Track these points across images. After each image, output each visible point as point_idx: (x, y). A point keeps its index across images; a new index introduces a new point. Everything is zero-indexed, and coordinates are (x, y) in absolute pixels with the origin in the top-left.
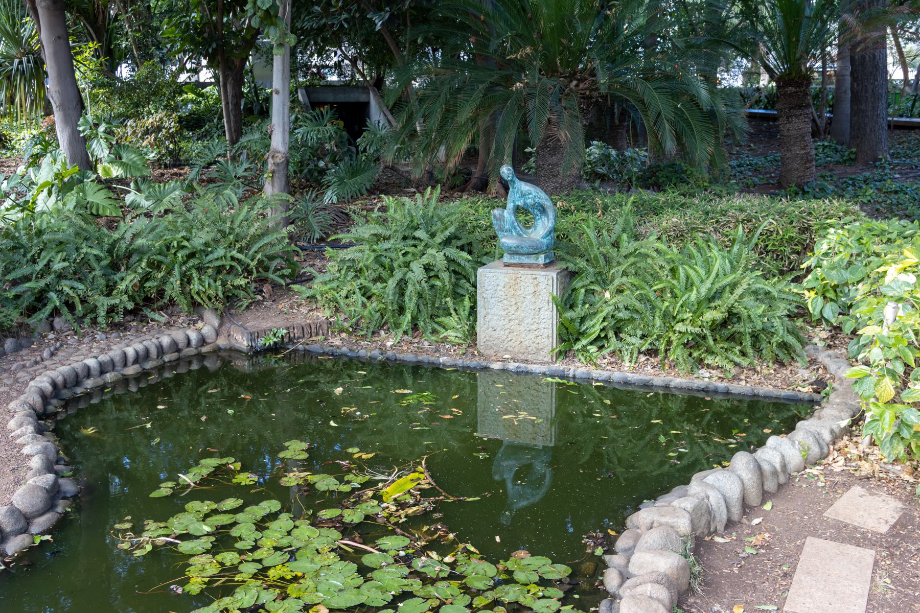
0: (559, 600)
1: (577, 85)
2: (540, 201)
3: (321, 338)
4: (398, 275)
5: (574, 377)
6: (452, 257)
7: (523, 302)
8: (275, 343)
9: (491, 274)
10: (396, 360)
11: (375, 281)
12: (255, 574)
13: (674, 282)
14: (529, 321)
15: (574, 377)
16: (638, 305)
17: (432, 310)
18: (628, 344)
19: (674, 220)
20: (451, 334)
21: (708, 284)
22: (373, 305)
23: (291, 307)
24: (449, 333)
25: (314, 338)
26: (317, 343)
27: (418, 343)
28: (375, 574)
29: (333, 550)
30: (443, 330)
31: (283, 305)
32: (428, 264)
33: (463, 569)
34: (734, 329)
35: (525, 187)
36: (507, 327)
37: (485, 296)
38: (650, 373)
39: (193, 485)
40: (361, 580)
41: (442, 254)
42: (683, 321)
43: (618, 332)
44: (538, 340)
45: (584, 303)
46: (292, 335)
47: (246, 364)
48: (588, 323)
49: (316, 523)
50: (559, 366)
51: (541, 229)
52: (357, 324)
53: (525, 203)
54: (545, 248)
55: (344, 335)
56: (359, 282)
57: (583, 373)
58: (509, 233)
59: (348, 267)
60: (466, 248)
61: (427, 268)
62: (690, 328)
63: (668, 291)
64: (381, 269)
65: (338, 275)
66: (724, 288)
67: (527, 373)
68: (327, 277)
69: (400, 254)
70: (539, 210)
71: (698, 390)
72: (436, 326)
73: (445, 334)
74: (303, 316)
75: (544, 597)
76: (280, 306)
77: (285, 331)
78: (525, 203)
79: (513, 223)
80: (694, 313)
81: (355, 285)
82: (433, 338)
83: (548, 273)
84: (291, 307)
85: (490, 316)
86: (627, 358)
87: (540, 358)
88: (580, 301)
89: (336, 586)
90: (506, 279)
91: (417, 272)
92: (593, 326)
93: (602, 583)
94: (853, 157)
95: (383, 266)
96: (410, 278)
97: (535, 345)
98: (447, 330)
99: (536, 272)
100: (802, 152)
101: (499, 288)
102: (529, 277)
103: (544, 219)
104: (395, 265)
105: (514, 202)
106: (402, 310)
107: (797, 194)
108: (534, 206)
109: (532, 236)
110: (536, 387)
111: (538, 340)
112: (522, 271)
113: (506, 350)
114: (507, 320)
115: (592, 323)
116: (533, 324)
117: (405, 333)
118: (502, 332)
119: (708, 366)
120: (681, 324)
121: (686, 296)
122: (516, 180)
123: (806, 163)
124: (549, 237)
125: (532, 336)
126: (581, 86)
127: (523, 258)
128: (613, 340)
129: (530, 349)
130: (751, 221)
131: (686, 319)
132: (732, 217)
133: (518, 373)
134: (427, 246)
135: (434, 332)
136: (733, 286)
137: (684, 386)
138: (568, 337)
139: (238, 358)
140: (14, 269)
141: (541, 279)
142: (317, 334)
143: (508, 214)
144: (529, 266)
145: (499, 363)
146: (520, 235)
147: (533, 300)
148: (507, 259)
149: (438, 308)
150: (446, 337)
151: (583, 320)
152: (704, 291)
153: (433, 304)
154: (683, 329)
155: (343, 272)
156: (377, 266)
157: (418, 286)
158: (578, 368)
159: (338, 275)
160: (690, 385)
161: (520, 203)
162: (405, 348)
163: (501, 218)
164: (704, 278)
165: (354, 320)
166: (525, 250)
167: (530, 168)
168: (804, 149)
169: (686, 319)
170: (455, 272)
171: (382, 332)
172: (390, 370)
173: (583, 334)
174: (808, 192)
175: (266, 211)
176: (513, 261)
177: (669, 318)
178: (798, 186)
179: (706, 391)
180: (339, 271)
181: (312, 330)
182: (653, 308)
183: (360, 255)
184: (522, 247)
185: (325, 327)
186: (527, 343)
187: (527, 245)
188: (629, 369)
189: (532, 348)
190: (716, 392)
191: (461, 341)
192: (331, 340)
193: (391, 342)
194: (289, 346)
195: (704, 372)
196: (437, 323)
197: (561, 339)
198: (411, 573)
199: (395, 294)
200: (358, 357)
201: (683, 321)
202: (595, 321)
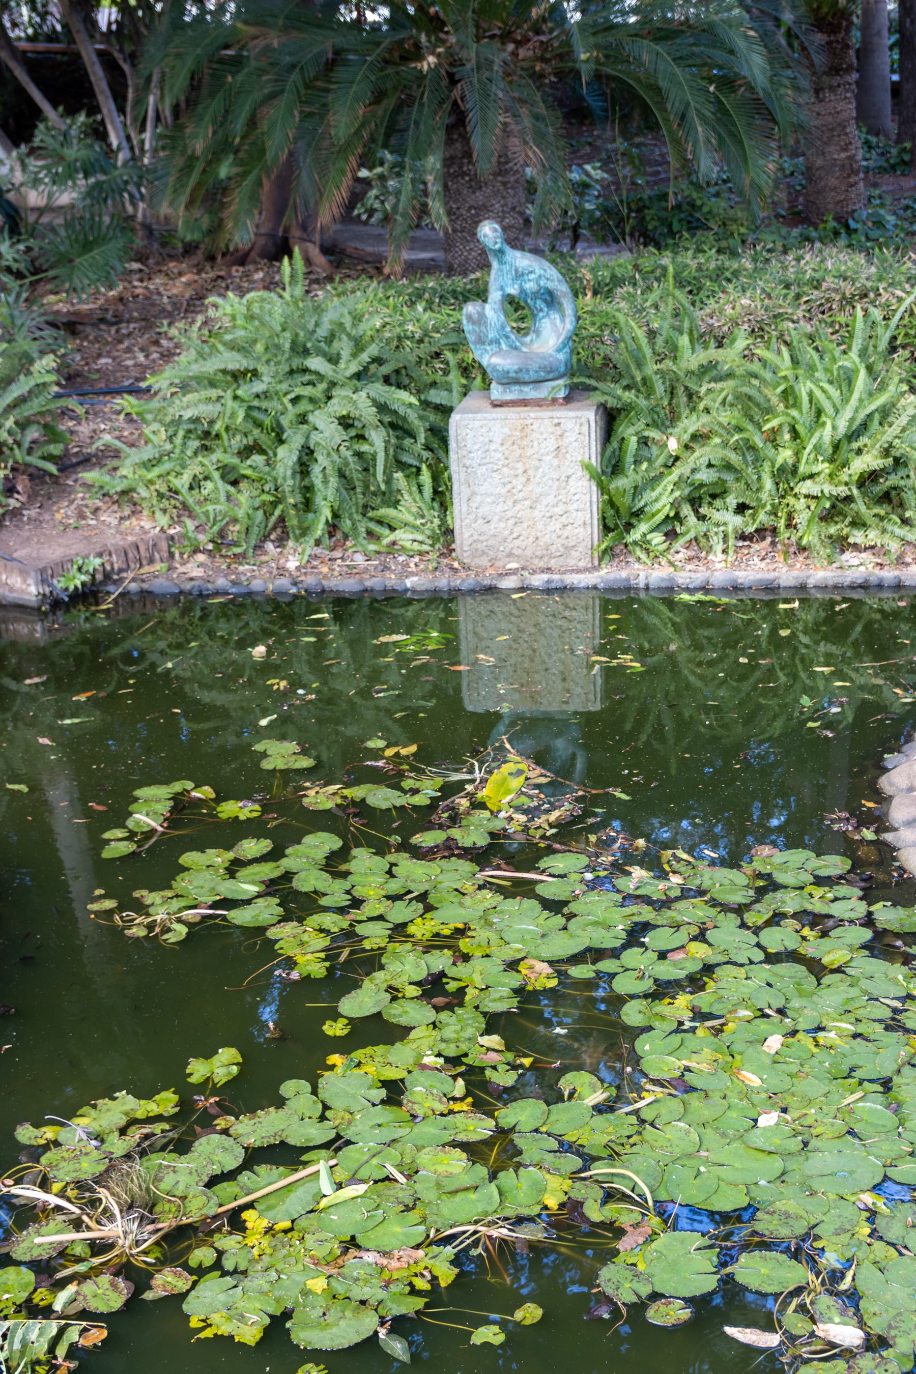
0: (861, 899)
1: (515, 54)
2: (550, 285)
3: (159, 566)
4: (295, 440)
5: (647, 588)
6: (382, 400)
7: (537, 469)
8: (84, 584)
9: (478, 424)
10: (323, 591)
11: (246, 452)
12: (390, 937)
13: (794, 413)
14: (551, 499)
15: (647, 588)
16: (734, 458)
17: (366, 497)
18: (717, 525)
19: (745, 301)
20: (403, 537)
21: (847, 413)
22: (245, 497)
23: (82, 516)
24: (399, 535)
25: (146, 569)
26: (158, 576)
27: (342, 558)
28: (573, 907)
29: (480, 888)
30: (387, 531)
31: (63, 512)
32: (348, 416)
33: (698, 882)
34: (888, 483)
35: (521, 260)
36: (509, 514)
37: (468, 463)
38: (757, 568)
39: (160, 829)
40: (560, 920)
41: (363, 394)
42: (812, 476)
43: (695, 502)
44: (566, 533)
45: (637, 462)
46: (108, 568)
47: (38, 628)
48: (649, 496)
49: (418, 853)
50: (609, 574)
51: (551, 336)
52: (222, 534)
53: (522, 290)
54: (562, 369)
55: (201, 557)
56: (214, 457)
57: (663, 580)
58: (494, 348)
59: (189, 431)
60: (393, 379)
61: (345, 422)
62: (828, 489)
63: (786, 429)
64: (256, 432)
65: (168, 447)
66: (870, 416)
67: (563, 590)
68: (148, 453)
69: (286, 400)
70: (545, 301)
71: (852, 587)
72: (373, 526)
73: (392, 537)
74: (115, 530)
75: (836, 899)
76: (58, 516)
77: (98, 561)
78: (522, 290)
79: (503, 328)
80: (831, 461)
81: (210, 461)
82: (372, 547)
83: (579, 413)
84: (82, 516)
86: (719, 547)
87: (572, 562)
88: (629, 459)
89: (529, 932)
90: (506, 430)
91: (326, 430)
92: (656, 500)
93: (901, 869)
94: (907, 157)
95: (259, 425)
96: (317, 444)
97: (561, 541)
98: (392, 529)
100: (843, 155)
101: (493, 446)
102: (547, 422)
103: (556, 316)
104: (285, 421)
105: (502, 288)
106: (307, 505)
107: (836, 234)
108: (536, 295)
109: (536, 348)
111: (566, 533)
112: (531, 414)
113: (510, 555)
115: (654, 494)
116: (556, 505)
117: (318, 543)
118: (502, 525)
119: (855, 547)
120: (809, 482)
121: (817, 435)
122: (507, 249)
123: (849, 176)
124: (567, 350)
125: (555, 525)
126: (522, 53)
127: (526, 389)
128: (692, 519)
129: (553, 549)
130: (866, 296)
131: (818, 474)
132: (836, 291)
133: (548, 591)
134: (333, 384)
136: (886, 413)
137: (830, 583)
138: (617, 521)
139: (15, 620)
141: (568, 425)
142: (151, 561)
143: (492, 311)
144: (538, 403)
145: (513, 578)
146: (516, 348)
147: (556, 462)
148: (497, 392)
149: (374, 494)
150: (394, 543)
151: (637, 491)
152: (843, 425)
153: (367, 487)
154: (815, 491)
155: (178, 440)
156: (250, 426)
157: (335, 457)
158: (645, 573)
159: (168, 447)
160: (840, 580)
161: (513, 290)
162: (325, 570)
163: (480, 320)
164: (838, 401)
165: (216, 528)
166: (533, 376)
167: (371, 212)
168: (845, 150)
169: (818, 474)
170: (393, 426)
171: (269, 546)
172: (284, 612)
173: (638, 514)
174: (856, 231)
175: (336, 344)
176: (509, 397)
177: (787, 475)
178: (837, 219)
179: (864, 586)
180: (171, 438)
181: (137, 555)
182: (758, 460)
183: (218, 407)
184: (528, 371)
185: (164, 545)
187: (535, 366)
188: (716, 565)
190: (880, 586)
191: (425, 548)
192: (182, 569)
193: (291, 565)
194: (111, 588)
195: (849, 557)
196: (371, 519)
197: (607, 529)
198: (624, 898)
199: (294, 474)
200: (250, 594)
201: (812, 476)
202: (659, 490)
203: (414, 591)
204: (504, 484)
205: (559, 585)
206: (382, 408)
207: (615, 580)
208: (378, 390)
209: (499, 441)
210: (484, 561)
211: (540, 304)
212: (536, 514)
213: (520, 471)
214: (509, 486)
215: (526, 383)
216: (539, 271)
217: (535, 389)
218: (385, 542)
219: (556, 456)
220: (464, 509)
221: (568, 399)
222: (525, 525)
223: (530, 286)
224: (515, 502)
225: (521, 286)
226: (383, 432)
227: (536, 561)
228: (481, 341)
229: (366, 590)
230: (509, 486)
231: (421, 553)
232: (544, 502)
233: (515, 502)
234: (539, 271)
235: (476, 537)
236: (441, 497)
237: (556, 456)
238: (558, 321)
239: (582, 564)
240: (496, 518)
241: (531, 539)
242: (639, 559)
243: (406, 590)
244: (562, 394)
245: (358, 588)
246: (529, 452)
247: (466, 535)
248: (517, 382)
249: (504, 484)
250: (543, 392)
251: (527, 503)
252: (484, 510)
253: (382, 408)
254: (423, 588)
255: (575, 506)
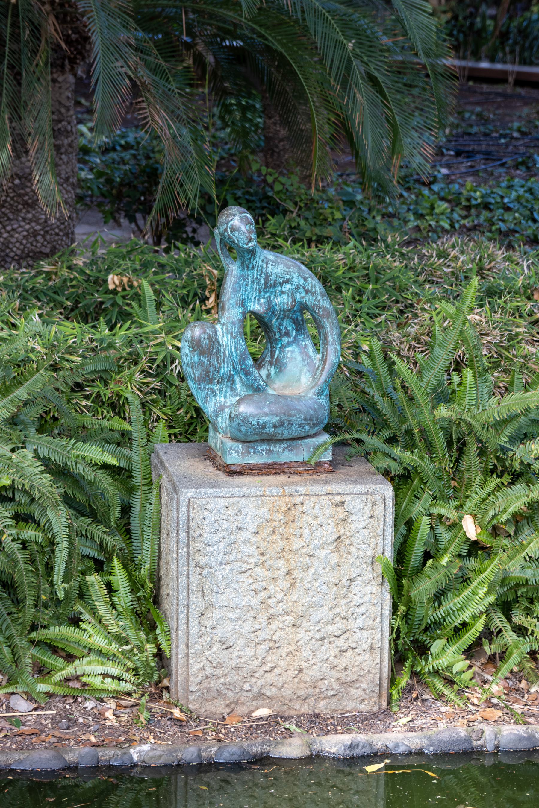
2: (309, 300)
7: (306, 568)
14: (324, 613)
24: (81, 666)
30: (60, 662)
35: (275, 264)
36: (262, 635)
37: (203, 561)
44: (344, 662)
48: (452, 602)
51: (302, 376)
53: (270, 306)
73: (69, 670)
78: (270, 306)
79: (243, 360)
85: (217, 613)
87: (350, 705)
90: (263, 512)
92: (461, 609)
97: (335, 674)
98: (70, 658)
99: (340, 488)
101: (243, 536)
102: (324, 500)
105: (242, 304)
108: (285, 313)
110: (336, 781)
113: (260, 696)
114: (263, 619)
116: (332, 622)
118: (250, 652)
122: (259, 250)
125: (328, 651)
127: (278, 449)
129: (323, 686)
135: (42, 671)
140: (57, 148)
141: (354, 504)
144: (294, 469)
147: (334, 559)
163: (208, 349)
166: (295, 430)
176: (253, 460)
184: (290, 424)
186: (315, 672)
187: (299, 418)
189: (330, 683)
203: (146, 768)
204: (256, 592)
205: (367, 751)
206: (59, 472)
207: (451, 742)
208: (45, 444)
209: (252, 528)
210: (220, 707)
211: (288, 325)
212: (302, 635)
213: (281, 572)
214: (263, 595)
215: (280, 441)
216: (297, 280)
217: (290, 449)
218: (58, 677)
219: (336, 550)
220: (194, 628)
221: (334, 465)
222: (283, 652)
223: (282, 301)
224: (271, 617)
225: (269, 301)
226: (64, 511)
227: (297, 705)
228: (207, 378)
229: (68, 768)
230: (263, 595)
231: (117, 696)
232: (314, 618)
233: (271, 617)
234: (297, 280)
235: (209, 671)
236: (149, 610)
237: (336, 550)
238: (311, 349)
239: (364, 707)
240: (241, 642)
241: (292, 673)
242: (440, 697)
243: (134, 765)
244: (328, 456)
245: (55, 765)
246: (296, 544)
247: (194, 668)
248: (271, 440)
249: (256, 592)
250: (302, 454)
251: (289, 619)
252: (225, 630)
253: (59, 472)
254: (160, 762)
255: (360, 622)
